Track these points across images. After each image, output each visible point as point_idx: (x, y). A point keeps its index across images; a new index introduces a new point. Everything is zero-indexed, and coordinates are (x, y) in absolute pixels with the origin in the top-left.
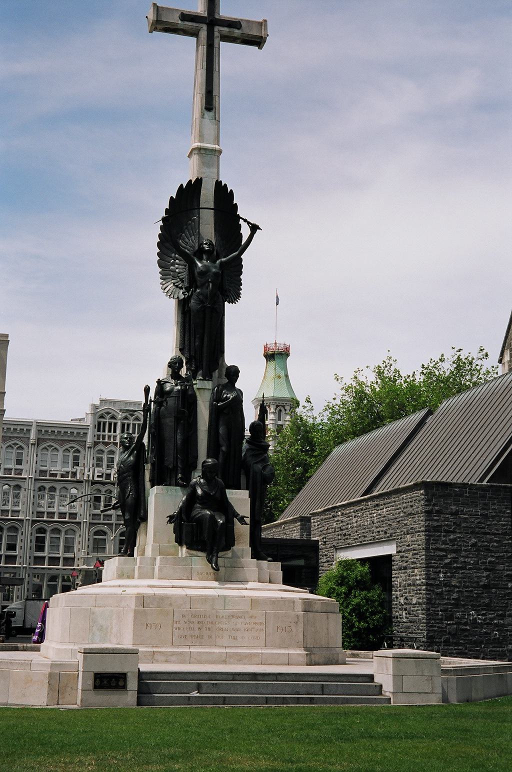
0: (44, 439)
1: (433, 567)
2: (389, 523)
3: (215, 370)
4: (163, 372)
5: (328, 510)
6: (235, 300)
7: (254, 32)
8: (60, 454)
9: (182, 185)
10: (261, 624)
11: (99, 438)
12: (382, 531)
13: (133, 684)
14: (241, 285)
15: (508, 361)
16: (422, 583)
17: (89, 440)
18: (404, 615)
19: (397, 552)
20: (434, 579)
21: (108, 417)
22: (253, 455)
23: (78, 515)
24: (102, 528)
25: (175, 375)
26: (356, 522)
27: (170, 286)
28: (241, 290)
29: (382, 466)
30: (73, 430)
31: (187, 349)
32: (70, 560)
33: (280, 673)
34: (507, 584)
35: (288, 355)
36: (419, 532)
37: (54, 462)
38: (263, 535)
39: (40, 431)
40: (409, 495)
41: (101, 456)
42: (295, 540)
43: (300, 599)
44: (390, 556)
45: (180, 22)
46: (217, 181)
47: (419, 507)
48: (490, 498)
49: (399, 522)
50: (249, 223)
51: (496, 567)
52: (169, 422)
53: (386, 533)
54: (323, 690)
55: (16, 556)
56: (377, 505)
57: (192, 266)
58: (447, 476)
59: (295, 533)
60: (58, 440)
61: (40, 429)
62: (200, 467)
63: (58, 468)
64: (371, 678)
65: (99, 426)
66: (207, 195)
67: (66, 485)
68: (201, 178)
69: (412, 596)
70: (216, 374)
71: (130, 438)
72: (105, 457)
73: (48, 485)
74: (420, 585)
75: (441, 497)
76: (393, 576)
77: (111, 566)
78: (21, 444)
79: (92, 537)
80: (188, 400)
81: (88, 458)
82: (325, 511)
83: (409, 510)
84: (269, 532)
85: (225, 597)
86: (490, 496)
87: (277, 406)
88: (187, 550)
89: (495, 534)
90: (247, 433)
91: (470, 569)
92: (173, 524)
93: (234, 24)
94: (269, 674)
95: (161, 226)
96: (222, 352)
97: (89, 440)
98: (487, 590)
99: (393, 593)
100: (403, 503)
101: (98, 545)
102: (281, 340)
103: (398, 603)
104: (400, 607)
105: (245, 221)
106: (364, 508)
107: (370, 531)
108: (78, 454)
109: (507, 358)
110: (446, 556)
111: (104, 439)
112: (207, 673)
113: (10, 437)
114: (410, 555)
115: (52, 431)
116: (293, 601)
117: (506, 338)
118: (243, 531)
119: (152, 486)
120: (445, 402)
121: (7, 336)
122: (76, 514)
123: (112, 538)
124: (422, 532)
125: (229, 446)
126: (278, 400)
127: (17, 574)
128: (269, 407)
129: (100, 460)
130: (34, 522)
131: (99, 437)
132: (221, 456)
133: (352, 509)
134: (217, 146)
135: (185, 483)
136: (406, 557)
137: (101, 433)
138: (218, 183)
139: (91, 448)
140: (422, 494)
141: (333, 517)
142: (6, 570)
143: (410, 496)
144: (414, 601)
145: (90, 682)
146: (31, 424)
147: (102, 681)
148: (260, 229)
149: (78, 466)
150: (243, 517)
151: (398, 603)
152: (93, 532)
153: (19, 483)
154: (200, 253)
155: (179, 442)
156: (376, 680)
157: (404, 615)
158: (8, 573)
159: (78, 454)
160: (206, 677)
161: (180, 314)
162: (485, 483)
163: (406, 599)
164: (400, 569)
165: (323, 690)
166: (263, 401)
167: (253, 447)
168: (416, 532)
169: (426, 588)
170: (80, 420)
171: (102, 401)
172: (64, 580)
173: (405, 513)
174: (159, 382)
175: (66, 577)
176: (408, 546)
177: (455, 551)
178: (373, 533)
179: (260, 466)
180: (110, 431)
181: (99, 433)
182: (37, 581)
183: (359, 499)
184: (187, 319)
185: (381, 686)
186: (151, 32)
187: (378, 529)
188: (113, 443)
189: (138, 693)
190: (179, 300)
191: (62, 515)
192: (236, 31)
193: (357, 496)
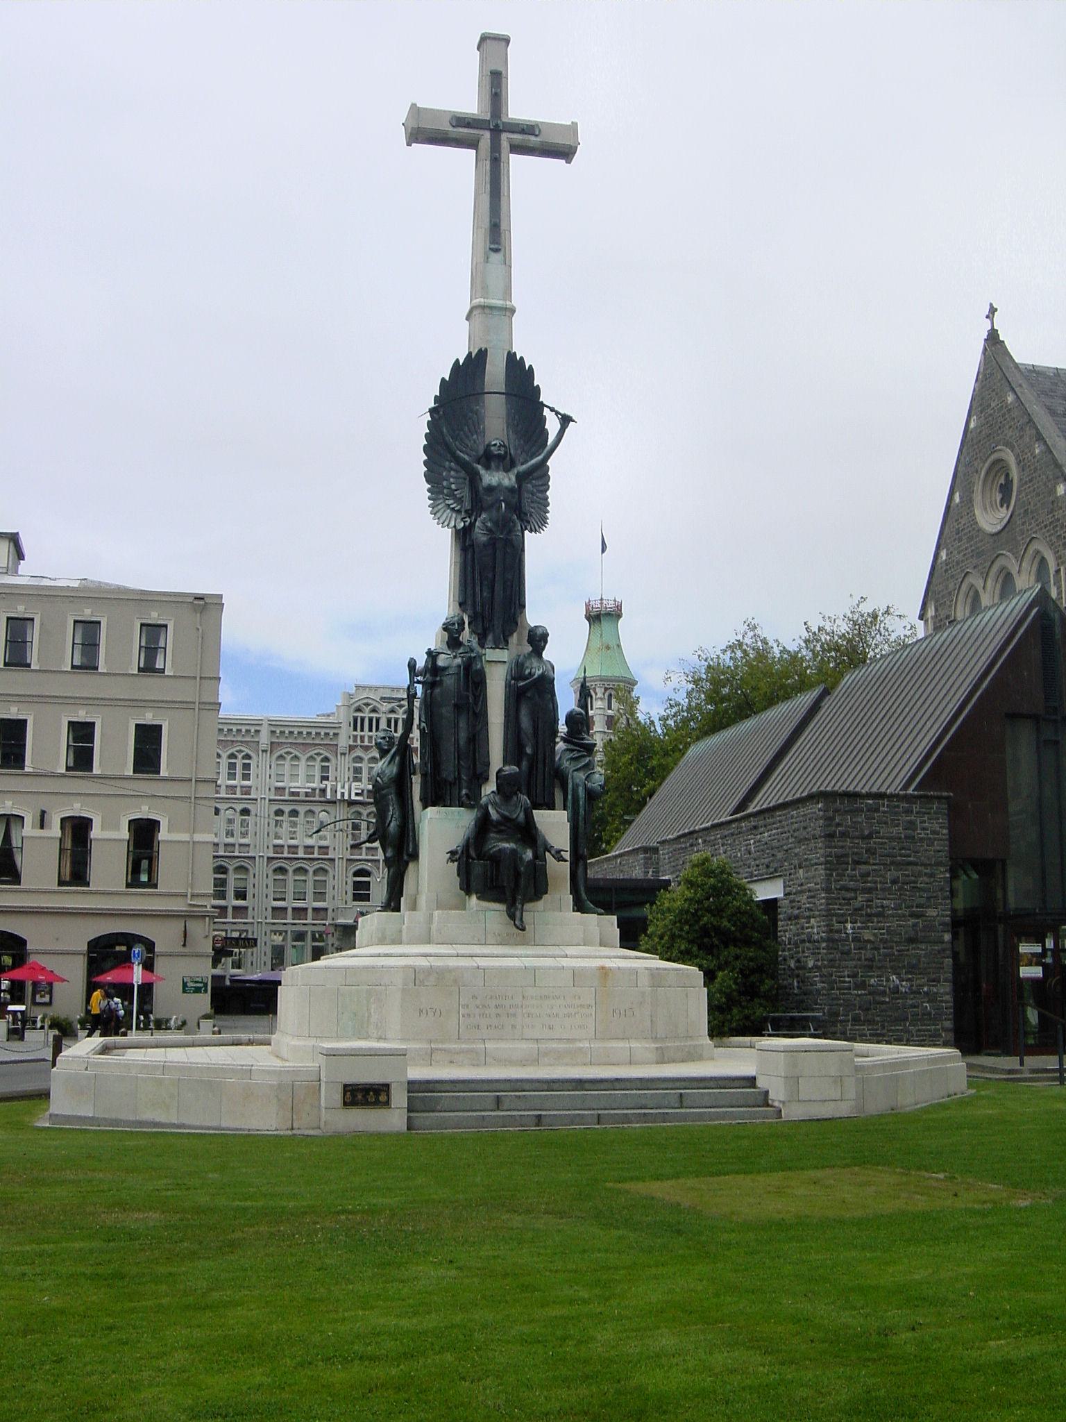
0: (278, 743)
1: (836, 915)
2: (773, 852)
3: (511, 634)
4: (432, 638)
5: (684, 835)
6: (540, 527)
7: (559, 140)
8: (303, 763)
9: (457, 361)
10: (589, 1006)
11: (355, 740)
12: (763, 865)
13: (399, 1098)
14: (548, 505)
15: (932, 617)
16: (821, 937)
17: (343, 742)
18: (796, 984)
19: (785, 895)
20: (839, 931)
21: (367, 709)
22: (572, 759)
23: (331, 849)
24: (364, 867)
25: (453, 642)
26: (725, 853)
27: (440, 507)
28: (548, 512)
29: (760, 770)
30: (318, 730)
31: (469, 602)
32: (322, 913)
33: (617, 1079)
34: (942, 936)
35: (619, 616)
36: (816, 864)
37: (294, 777)
38: (590, 874)
39: (273, 732)
40: (802, 811)
41: (360, 765)
42: (636, 880)
43: (647, 969)
44: (775, 900)
45: (451, 129)
46: (509, 353)
47: (817, 827)
48: (917, 813)
49: (787, 851)
50: (557, 413)
51: (926, 912)
52: (447, 712)
53: (768, 867)
54: (681, 1102)
55: (246, 908)
56: (755, 827)
57: (474, 478)
58: (839, 784)
59: (636, 871)
60: (300, 744)
61: (273, 729)
62: (493, 777)
63: (300, 784)
64: (751, 1081)
65: (356, 724)
66: (495, 372)
67: (313, 808)
68: (486, 350)
69: (807, 957)
70: (514, 639)
71: (389, 738)
72: (239, 763)
73: (287, 809)
74: (818, 942)
75: (846, 812)
76: (779, 929)
77: (372, 923)
78: (247, 751)
79: (351, 879)
80: (474, 679)
81: (341, 767)
82: (679, 837)
83: (804, 834)
84: (598, 869)
85: (535, 969)
86: (918, 810)
87: (606, 689)
88: (478, 901)
89: (925, 865)
90: (562, 728)
92: (456, 863)
93: (529, 129)
94: (602, 1081)
95: (428, 422)
96: (523, 606)
97: (343, 742)
98: (914, 946)
99: (780, 953)
100: (792, 823)
101: (361, 892)
102: (610, 595)
103: (786, 967)
104: (789, 973)
105: (552, 410)
106: (736, 832)
107: (744, 865)
108: (326, 764)
109: (931, 612)
110: (856, 898)
111: (362, 741)
112: (509, 1081)
113: (233, 741)
114: (804, 898)
115: (238, 730)
117: (929, 583)
118: (559, 870)
119: (425, 807)
120: (848, 677)
121: (221, 596)
122: (327, 847)
123: (378, 880)
124: (821, 864)
125: (536, 747)
126: (608, 680)
127: (250, 933)
128: (595, 690)
129: (358, 771)
130: (270, 859)
131: (355, 737)
132: (524, 764)
133: (718, 834)
134: (508, 303)
135: (471, 801)
136: (798, 902)
137: (359, 733)
138: (511, 356)
139: (266, 751)
140: (820, 810)
141: (692, 845)
142: (235, 927)
143: (802, 813)
144: (810, 964)
145: (338, 1097)
146: (260, 722)
147: (354, 1096)
148: (573, 421)
149: (328, 780)
150: (559, 852)
151: (786, 967)
152: (352, 872)
153: (249, 806)
154: (489, 459)
155: (462, 742)
156: (759, 1083)
157: (796, 984)
158: (236, 931)
159: (326, 764)
160: (508, 1086)
161: (458, 550)
162: (910, 791)
163: (798, 961)
164: (790, 919)
165: (681, 1102)
166: (585, 678)
167: (573, 747)
168: (812, 865)
169: (827, 946)
170: (329, 716)
171: (358, 687)
172: (314, 939)
173: (796, 837)
174: (429, 653)
175: (317, 936)
176: (802, 885)
177: (869, 891)
178: (749, 867)
179: (581, 776)
180: (370, 730)
181: (355, 733)
182: (278, 939)
183: (729, 818)
184: (469, 556)
185: (767, 1092)
186: (409, 144)
187: (757, 862)
188: (361, 746)
189: (408, 1111)
190: (456, 530)
191: (309, 849)
192: (533, 138)
193: (724, 815)
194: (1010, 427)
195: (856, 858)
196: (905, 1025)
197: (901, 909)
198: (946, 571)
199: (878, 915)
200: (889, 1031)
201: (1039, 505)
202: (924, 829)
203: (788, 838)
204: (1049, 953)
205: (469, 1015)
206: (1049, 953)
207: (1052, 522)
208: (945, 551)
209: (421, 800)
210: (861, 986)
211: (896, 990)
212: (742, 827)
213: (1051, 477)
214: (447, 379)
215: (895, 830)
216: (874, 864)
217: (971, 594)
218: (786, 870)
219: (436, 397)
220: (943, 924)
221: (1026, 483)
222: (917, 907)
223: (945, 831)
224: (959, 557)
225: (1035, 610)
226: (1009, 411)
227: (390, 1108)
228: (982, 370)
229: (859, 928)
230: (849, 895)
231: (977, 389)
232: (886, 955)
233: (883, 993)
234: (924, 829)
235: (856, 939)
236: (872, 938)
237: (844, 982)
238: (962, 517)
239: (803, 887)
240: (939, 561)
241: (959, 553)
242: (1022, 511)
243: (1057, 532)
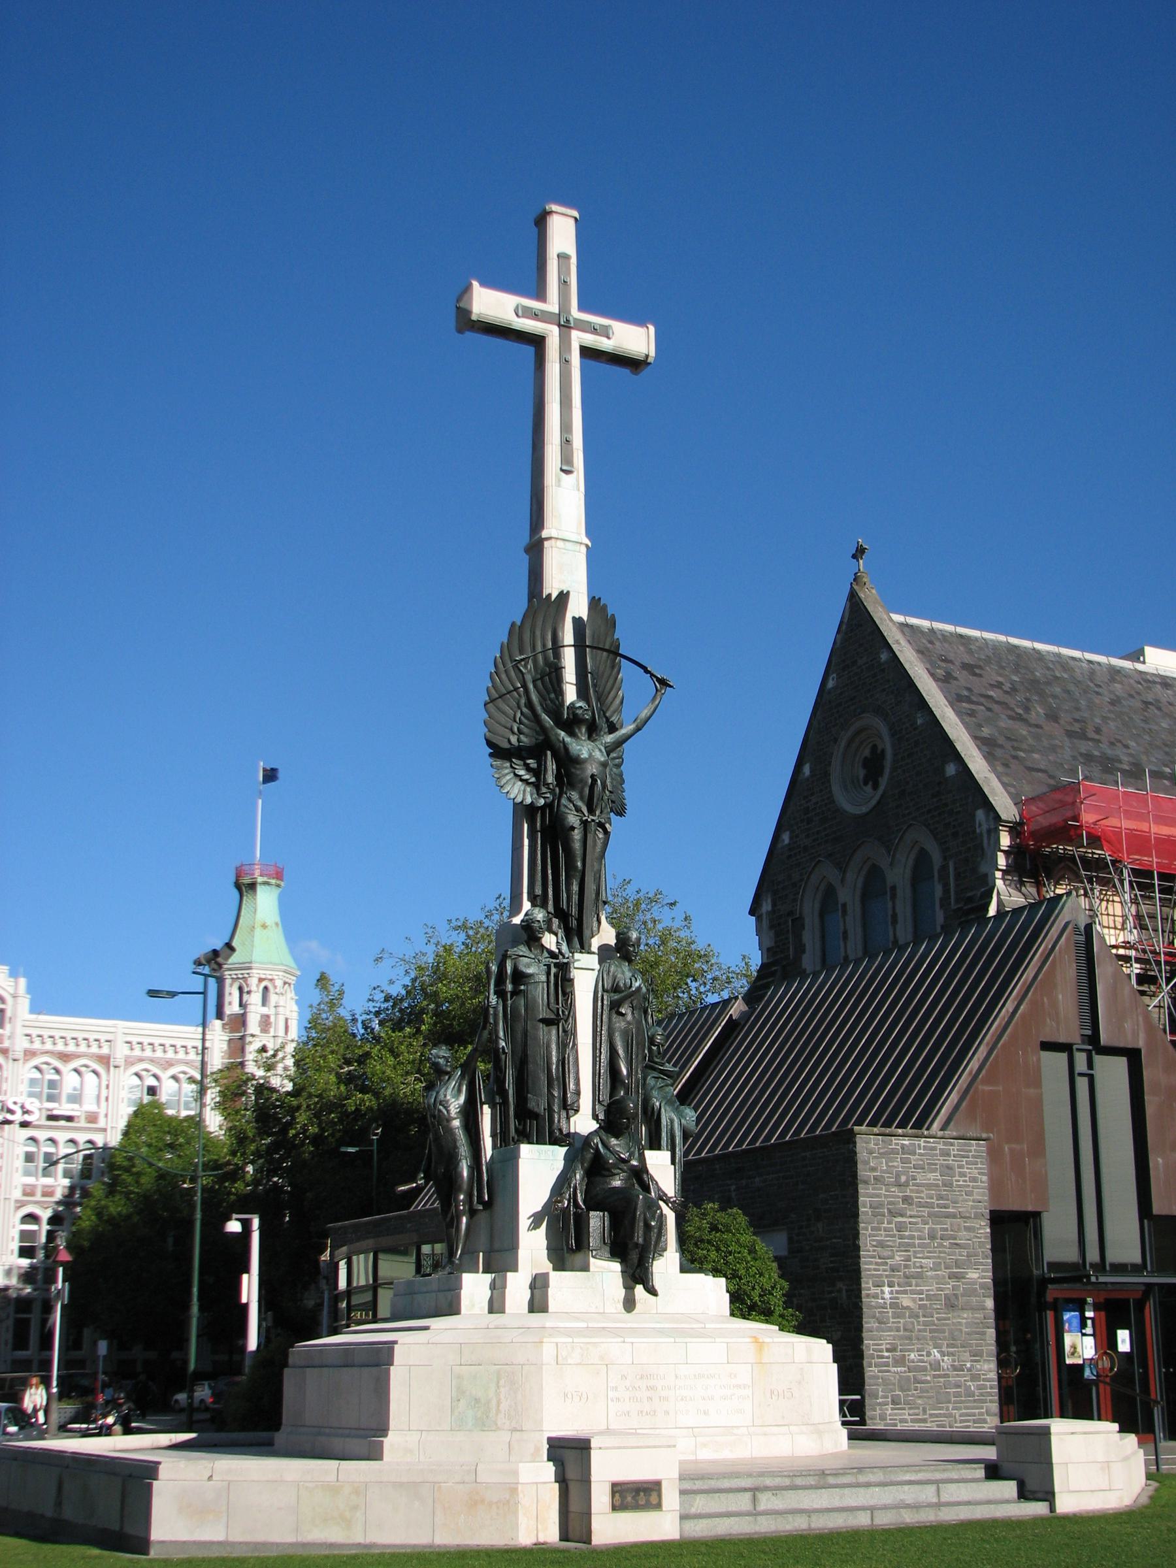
20: (876, 1296)
27: (508, 777)
34: (984, 1302)
51: (967, 1273)
68: (568, 592)
109: (766, 907)
147: (623, 1497)
194: (884, 690)
196: (947, 1409)
197: (940, 1270)
198: (790, 857)
200: (931, 1415)
202: (963, 1175)
204: (1089, 1322)
205: (618, 1399)
206: (1089, 1322)
208: (788, 833)
210: (900, 1361)
211: (936, 1366)
215: (931, 1176)
216: (911, 1217)
217: (822, 887)
220: (983, 1286)
223: (985, 1178)
226: (883, 670)
227: (662, 1510)
228: (846, 620)
229: (897, 1292)
231: (838, 642)
232: (925, 1324)
233: (924, 1369)
235: (894, 1305)
237: (882, 1357)
238: (812, 794)
240: (779, 845)
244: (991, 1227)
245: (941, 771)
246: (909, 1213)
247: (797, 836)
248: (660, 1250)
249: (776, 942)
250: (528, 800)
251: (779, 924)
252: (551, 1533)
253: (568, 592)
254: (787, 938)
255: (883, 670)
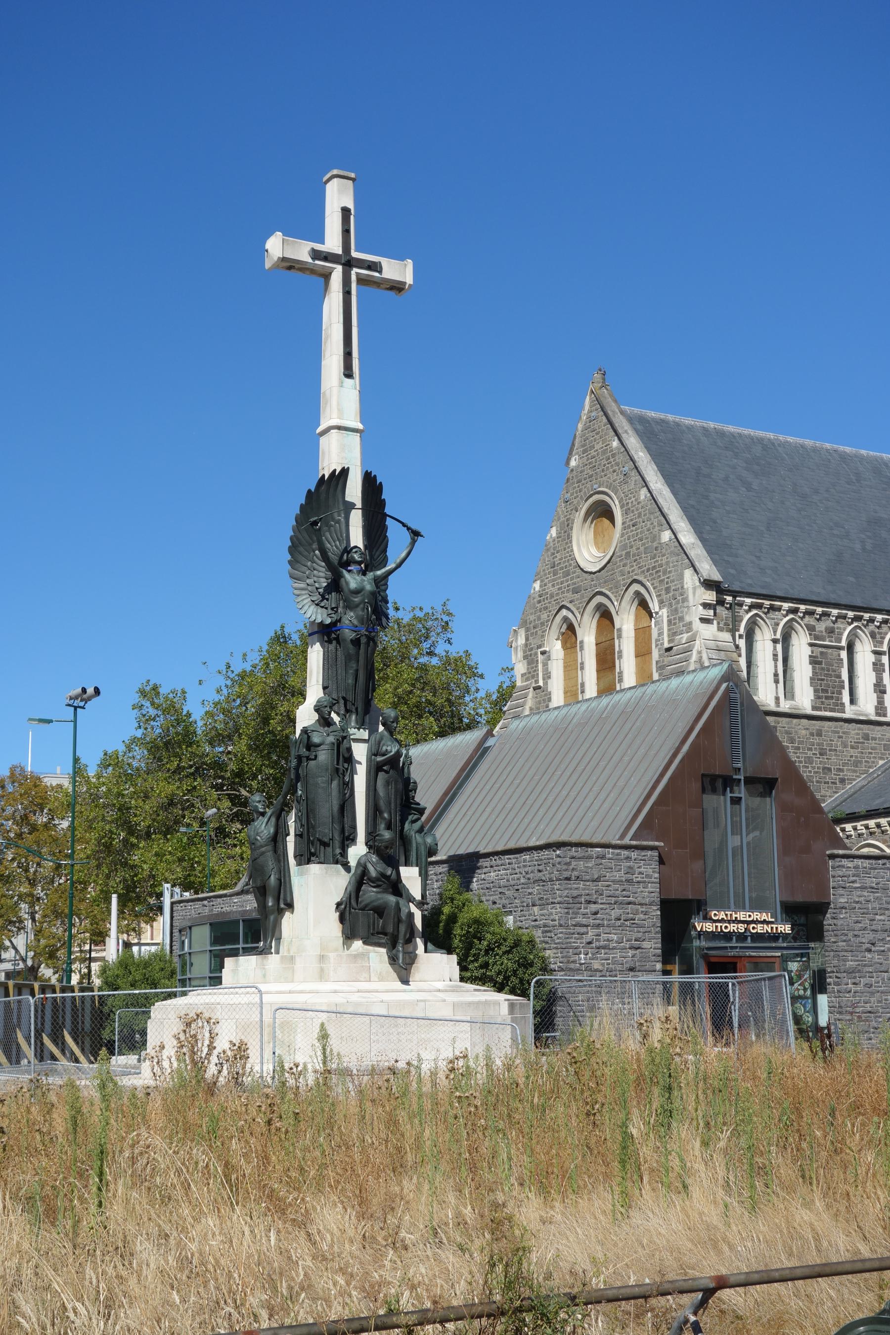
20: (574, 962)
27: (305, 602)
36: (553, 903)
50: (409, 529)
68: (348, 468)
91: (614, 948)
100: (524, 866)
110: (587, 933)
116: (497, 1003)
176: (536, 920)
177: (598, 926)
192: (377, 274)
194: (614, 471)
195: (588, 898)
198: (539, 602)
199: (604, 947)
201: (642, 549)
202: (640, 873)
203: (518, 879)
207: (654, 568)
209: (295, 857)
212: (462, 865)
213: (656, 524)
214: (313, 490)
215: (617, 874)
218: (517, 907)
219: (302, 505)
221: (629, 527)
222: (636, 940)
223: (657, 875)
224: (554, 590)
225: (724, 685)
226: (613, 455)
230: (583, 930)
234: (640, 873)
236: (600, 968)
237: (579, 1005)
239: (537, 923)
241: (553, 586)
242: (624, 553)
243: (659, 576)
244: (822, 925)
245: (655, 538)
246: (600, 901)
247: (545, 585)
248: (288, 834)
249: (528, 669)
250: (319, 620)
251: (531, 655)
252: (366, 745)
253: (348, 468)
254: (537, 666)
255: (613, 455)
